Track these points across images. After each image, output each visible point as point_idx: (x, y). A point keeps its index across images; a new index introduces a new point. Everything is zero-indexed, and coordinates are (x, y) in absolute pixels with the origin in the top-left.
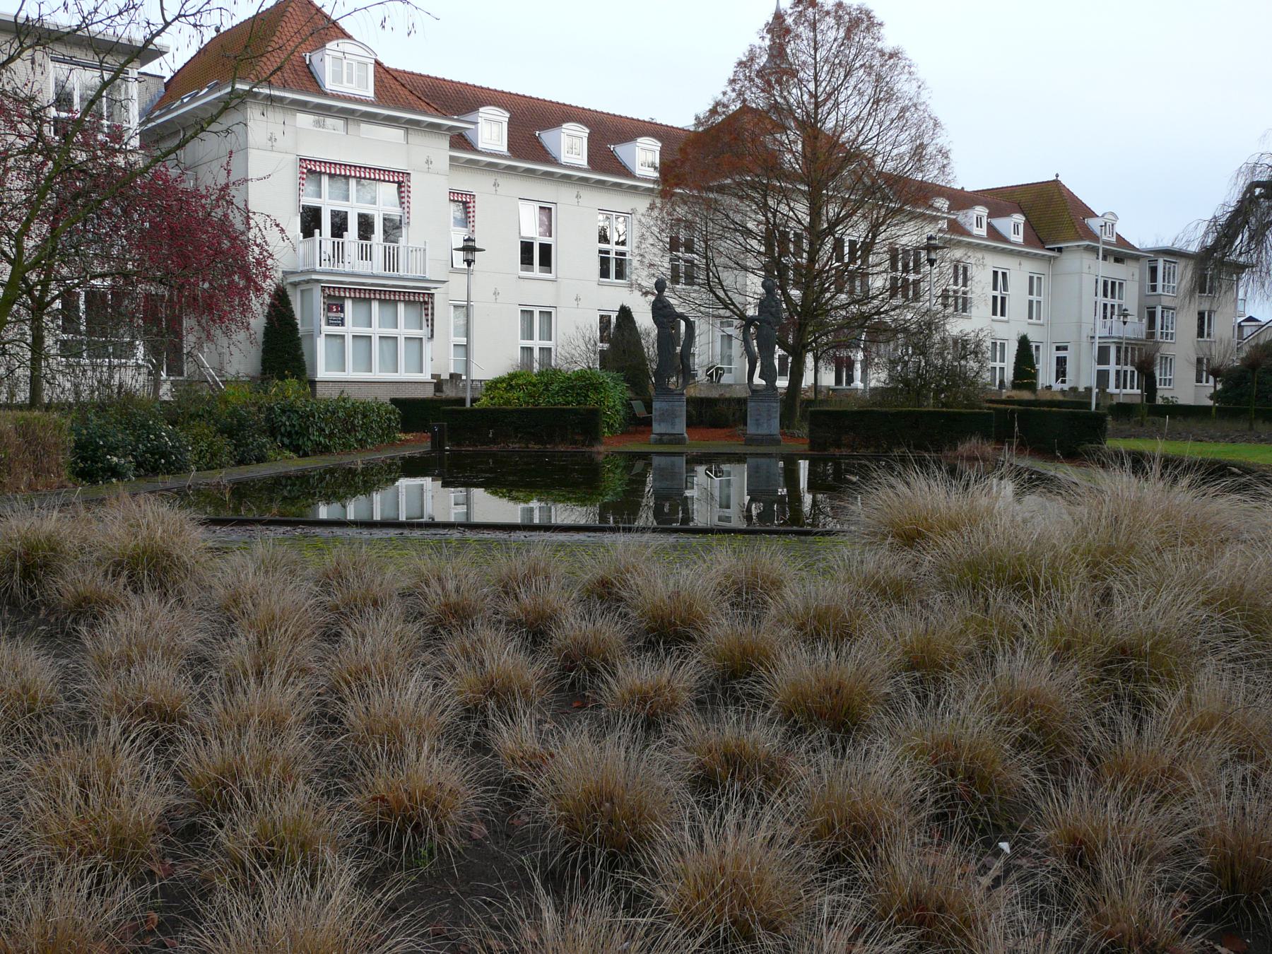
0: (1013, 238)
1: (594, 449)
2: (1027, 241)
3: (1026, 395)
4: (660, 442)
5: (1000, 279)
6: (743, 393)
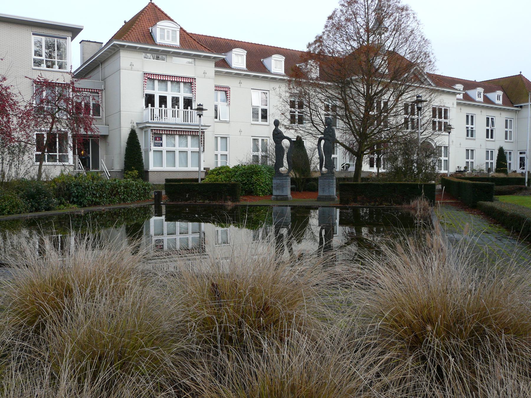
0: (497, 102)
1: (226, 204)
2: (504, 103)
3: (502, 175)
4: (277, 200)
5: (470, 119)
6: (317, 175)
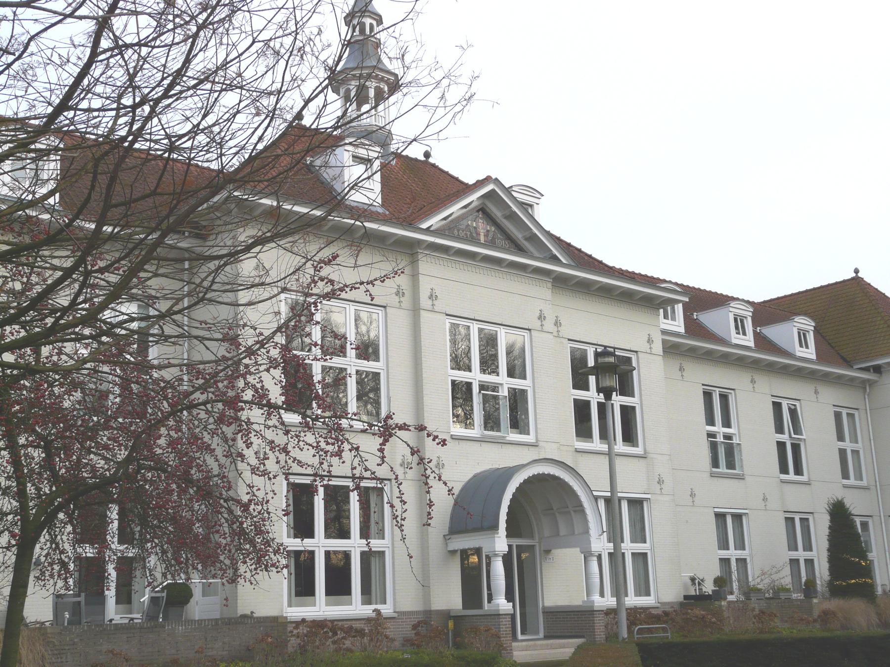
0: (800, 352)
